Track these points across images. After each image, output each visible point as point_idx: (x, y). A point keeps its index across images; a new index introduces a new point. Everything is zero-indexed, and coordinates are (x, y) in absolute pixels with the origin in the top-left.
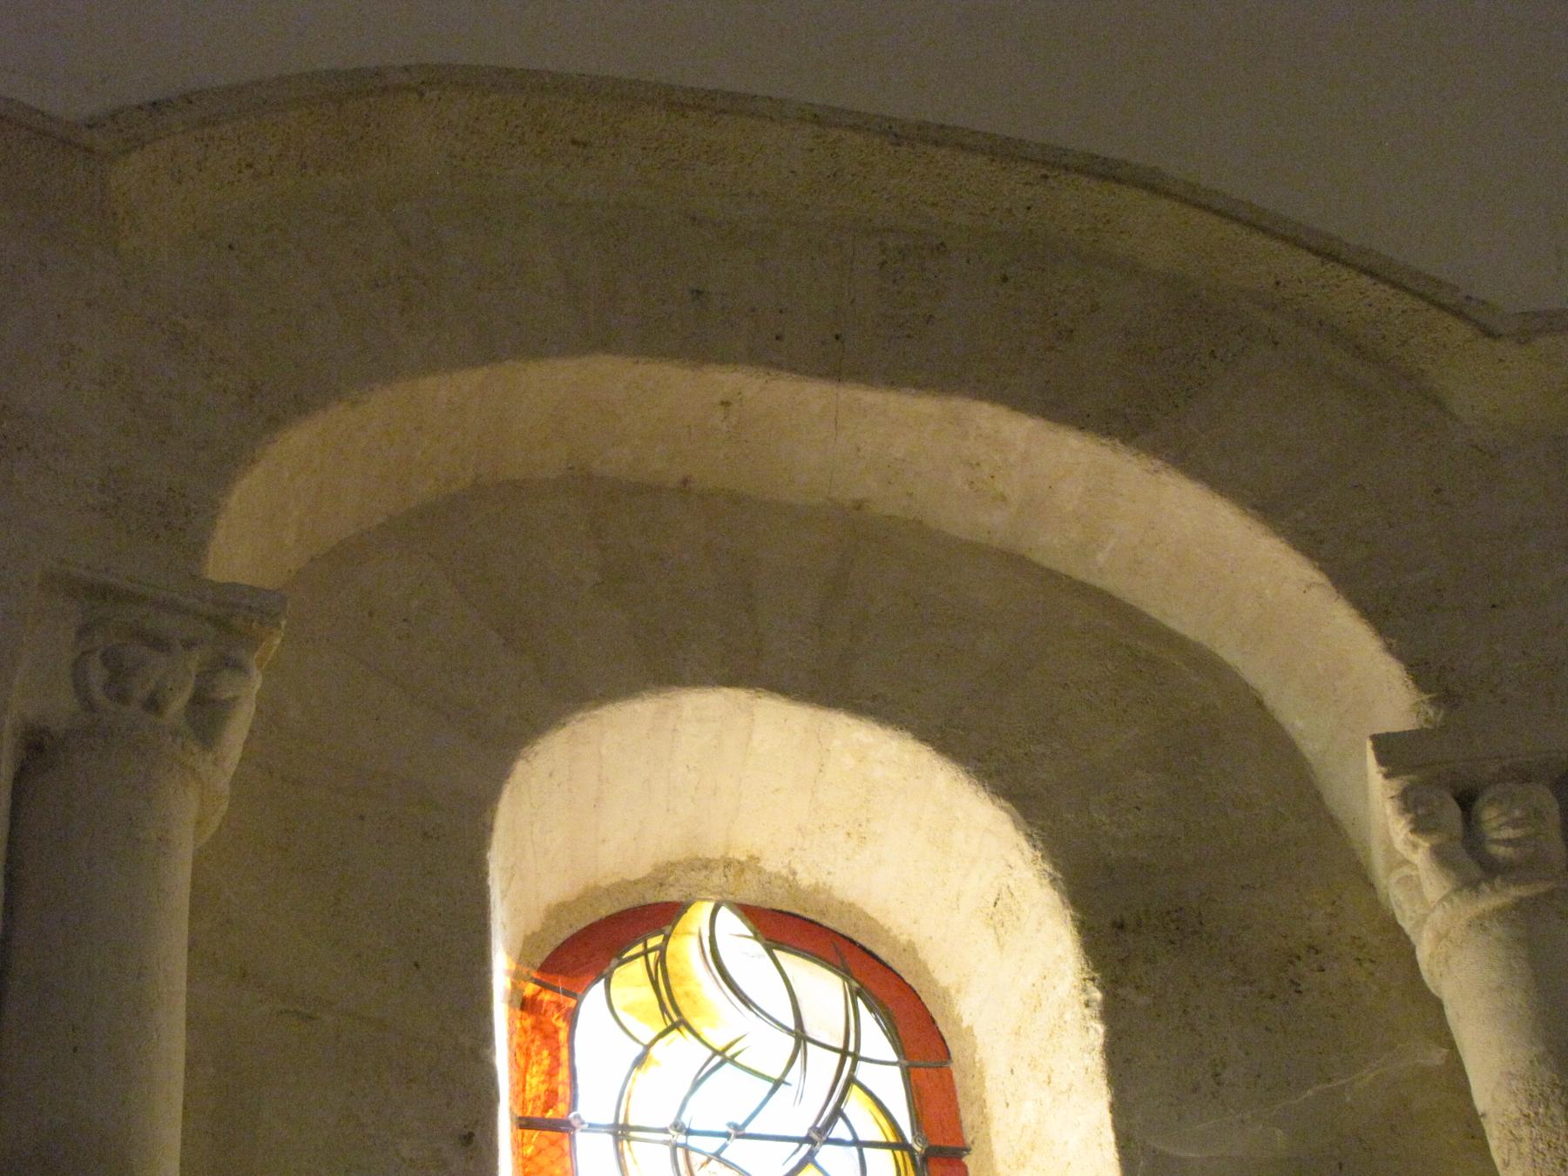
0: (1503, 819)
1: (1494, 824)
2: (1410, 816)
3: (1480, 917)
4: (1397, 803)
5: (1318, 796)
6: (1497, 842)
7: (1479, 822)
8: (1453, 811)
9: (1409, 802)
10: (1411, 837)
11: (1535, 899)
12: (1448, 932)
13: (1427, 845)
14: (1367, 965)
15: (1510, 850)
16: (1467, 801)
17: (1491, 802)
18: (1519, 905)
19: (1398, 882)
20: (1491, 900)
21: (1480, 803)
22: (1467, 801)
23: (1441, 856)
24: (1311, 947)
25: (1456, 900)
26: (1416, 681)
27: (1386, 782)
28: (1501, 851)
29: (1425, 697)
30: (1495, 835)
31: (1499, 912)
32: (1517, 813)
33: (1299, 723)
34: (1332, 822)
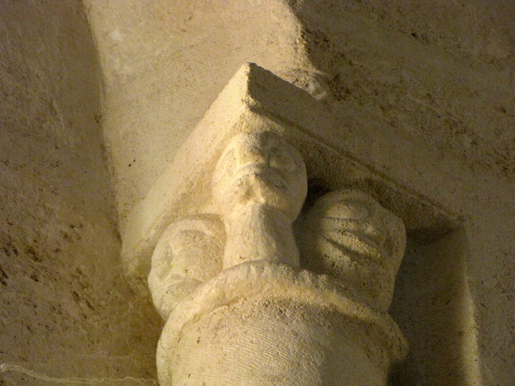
0: (352, 226)
1: (339, 225)
2: (261, 161)
3: (285, 303)
4: (253, 140)
5: (98, 119)
6: (335, 244)
7: (322, 215)
8: (300, 189)
9: (266, 147)
10: (252, 179)
11: (348, 320)
12: (235, 300)
13: (262, 200)
14: (83, 305)
15: (347, 258)
16: (318, 190)
17: (347, 202)
18: (332, 315)
19: (186, 232)
20: (305, 291)
21: (327, 199)
22: (318, 190)
23: (269, 216)
24: (30, 251)
25: (268, 270)
26: (309, 50)
27: (248, 113)
28: (334, 254)
29: (312, 70)
30: (336, 237)
31: (308, 312)
32: (370, 230)
33: (116, 35)
34: (103, 151)
